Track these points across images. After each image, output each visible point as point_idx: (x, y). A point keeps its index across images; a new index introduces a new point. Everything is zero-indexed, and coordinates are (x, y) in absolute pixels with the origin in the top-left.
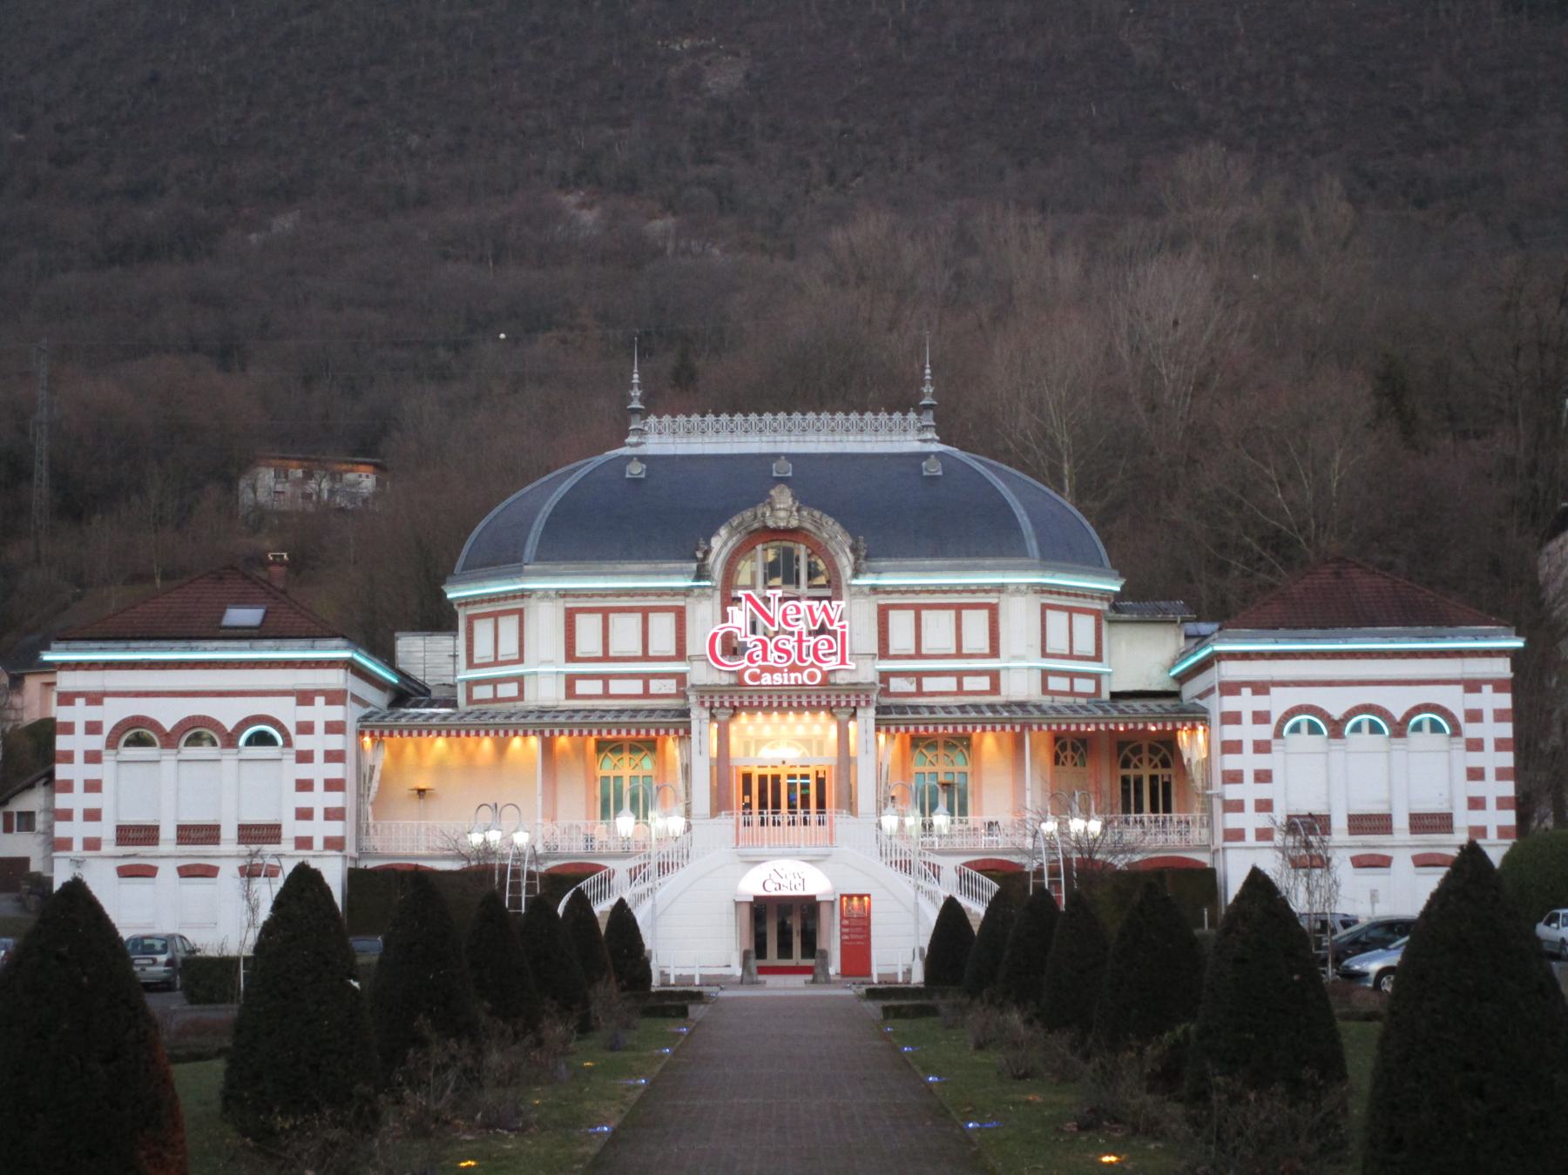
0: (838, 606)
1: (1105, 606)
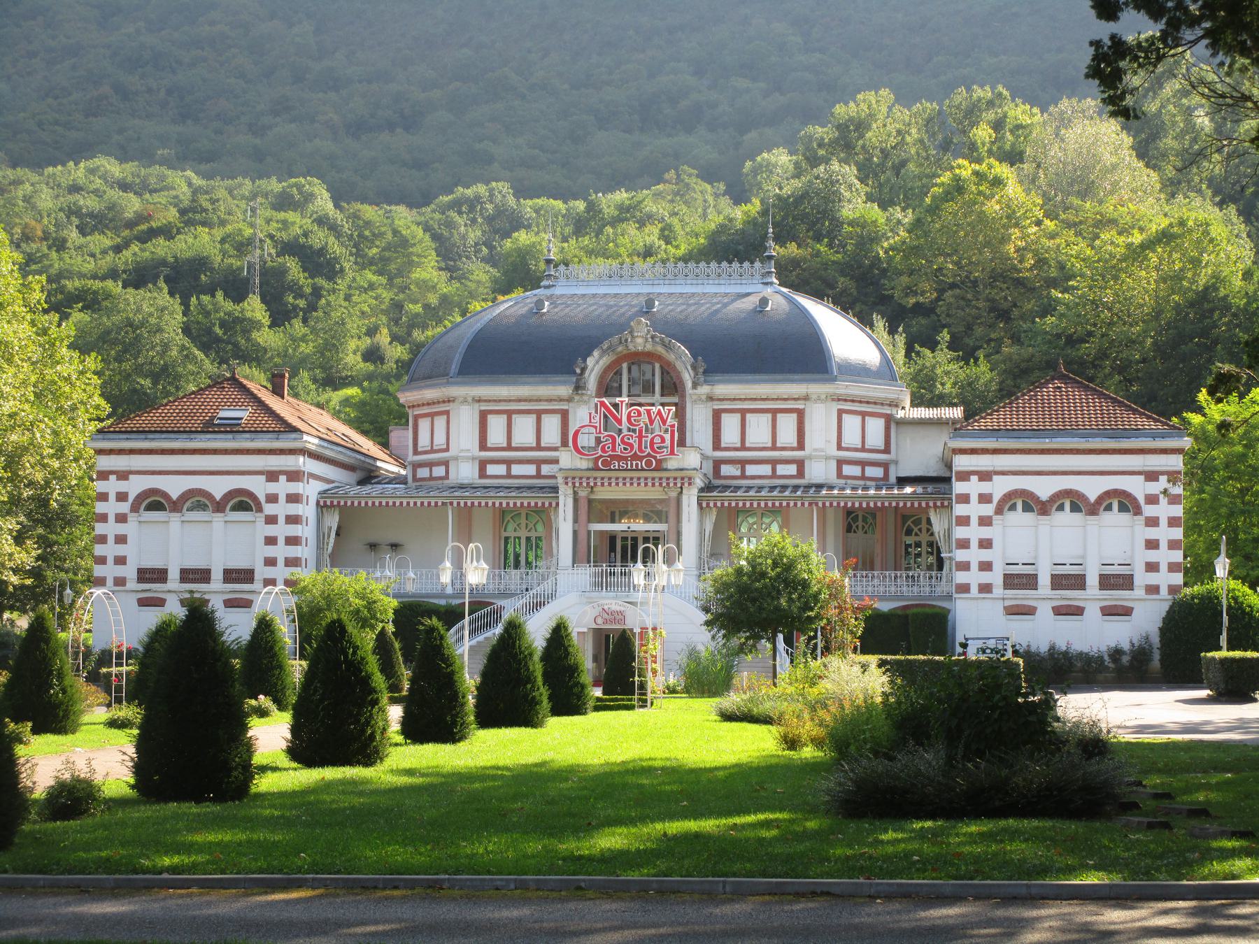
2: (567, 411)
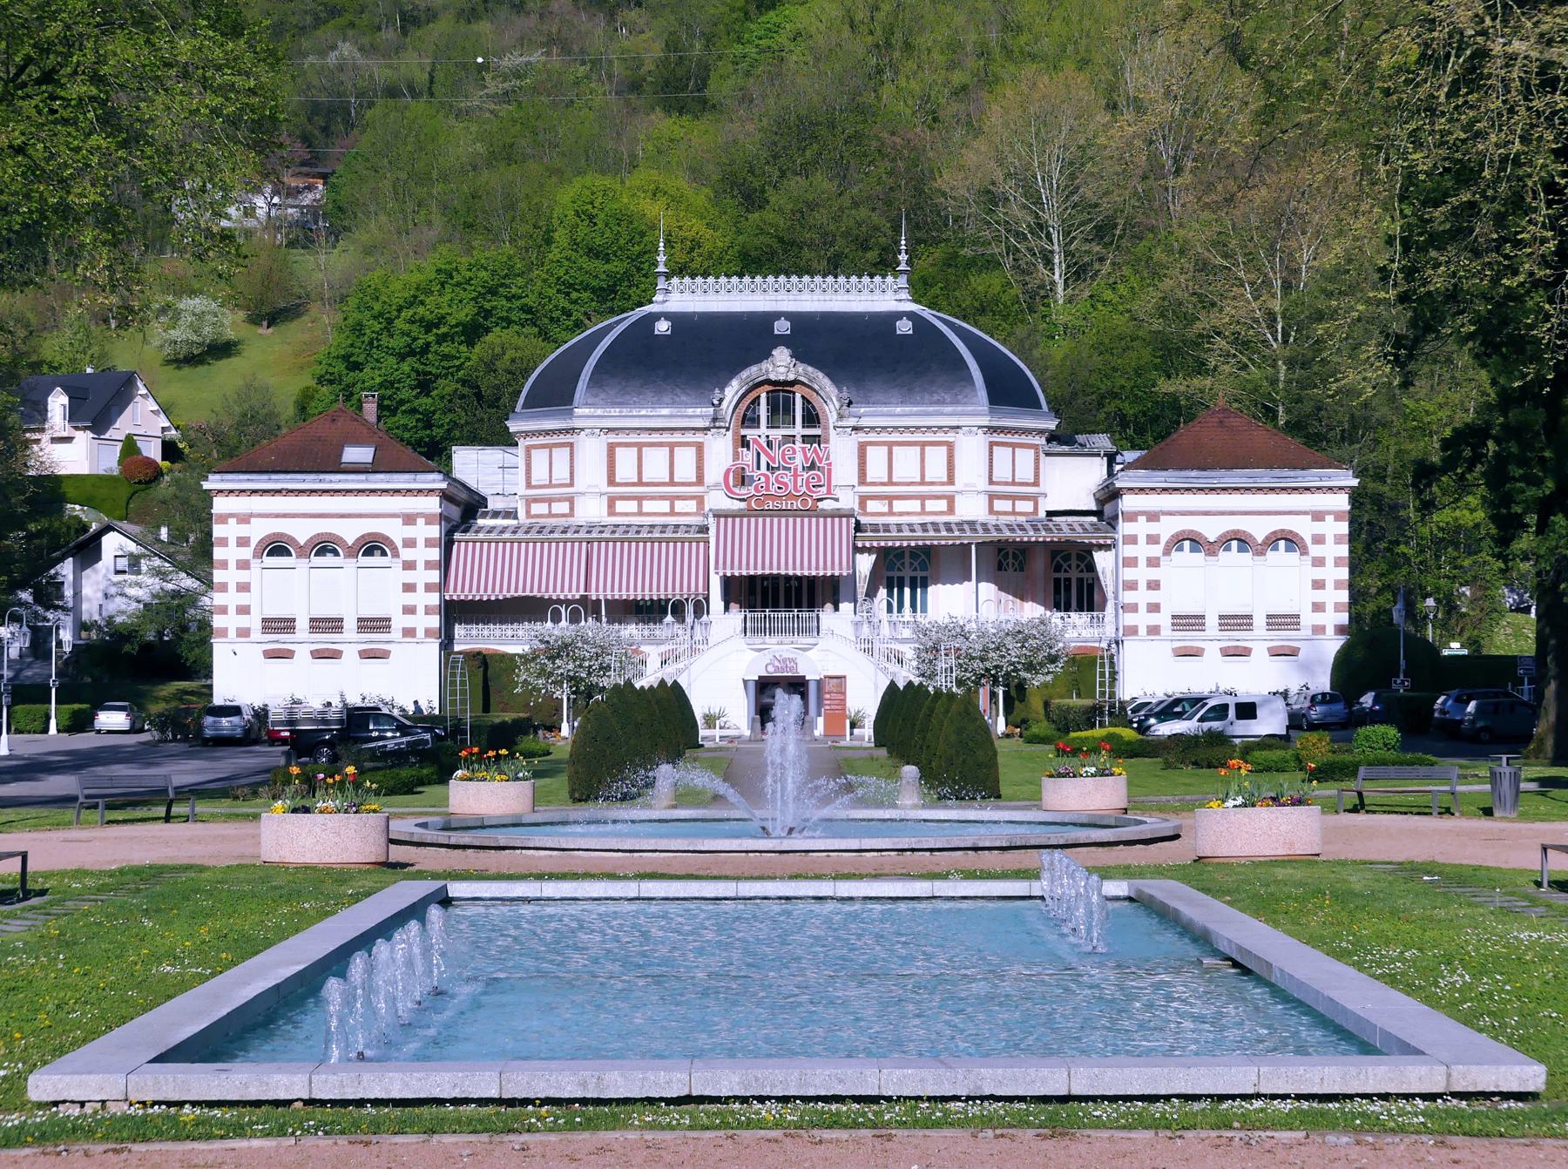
1: (1043, 441)
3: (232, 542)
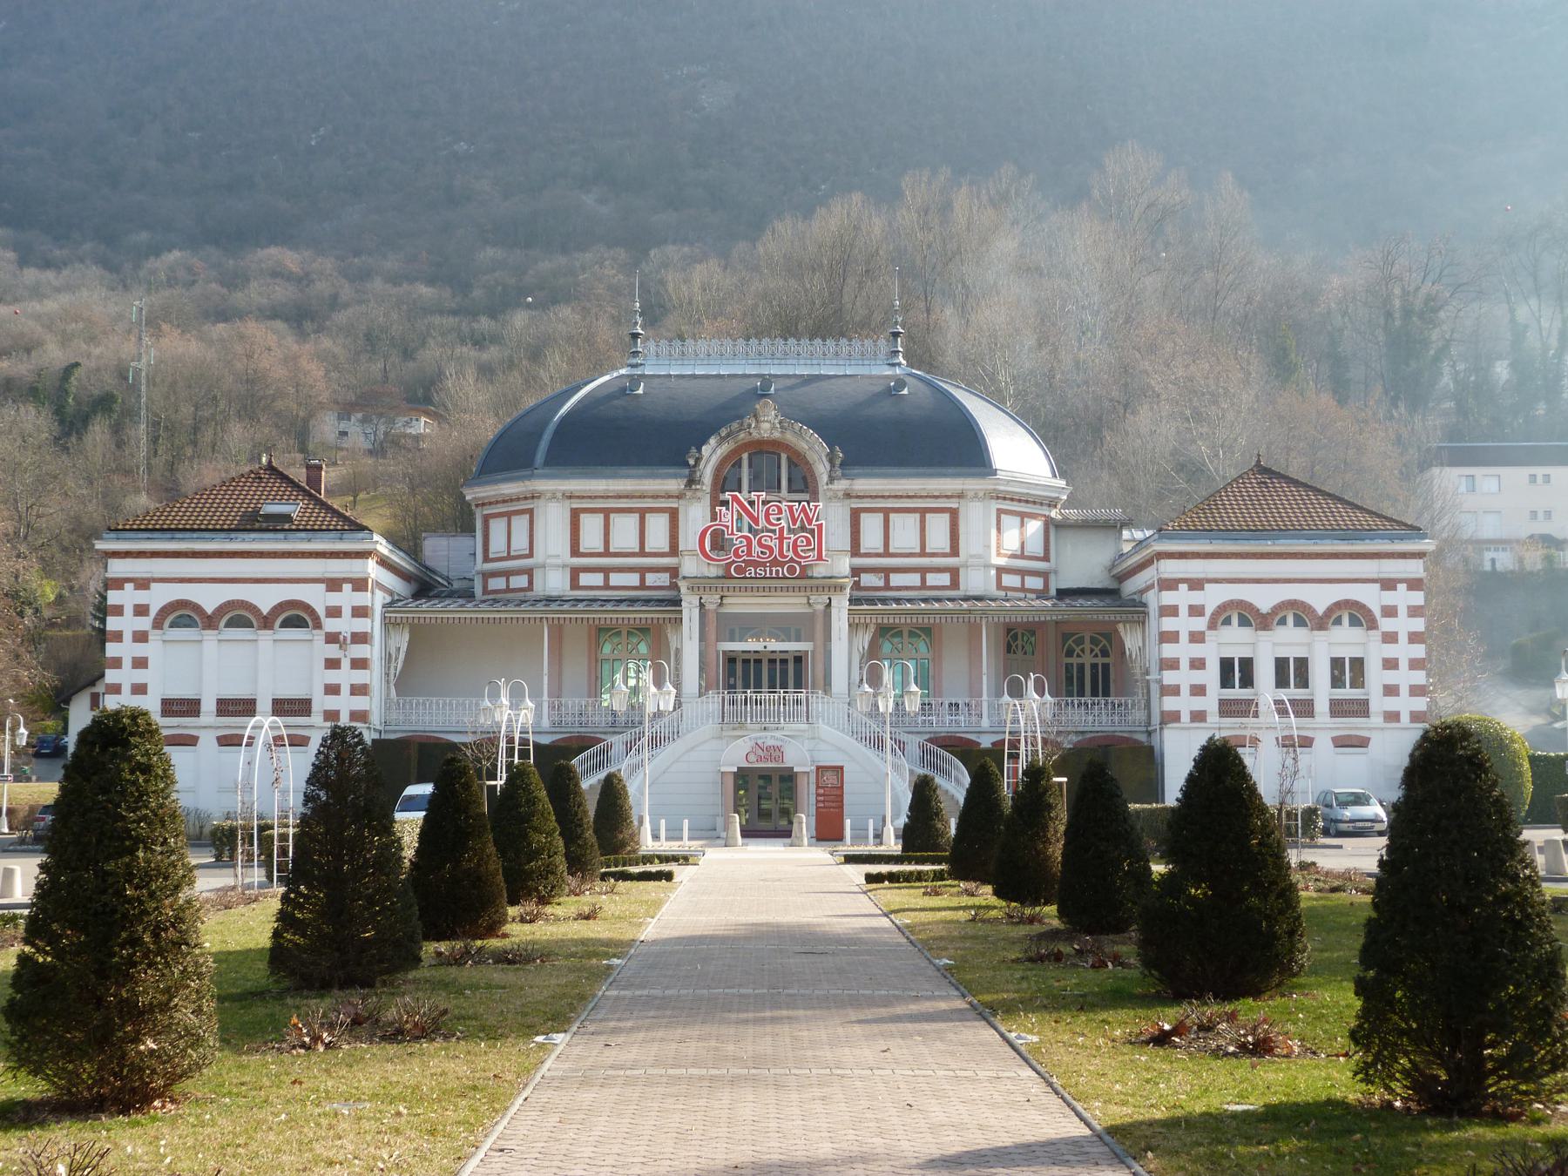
0: (816, 507)
2: (677, 509)
3: (128, 610)
